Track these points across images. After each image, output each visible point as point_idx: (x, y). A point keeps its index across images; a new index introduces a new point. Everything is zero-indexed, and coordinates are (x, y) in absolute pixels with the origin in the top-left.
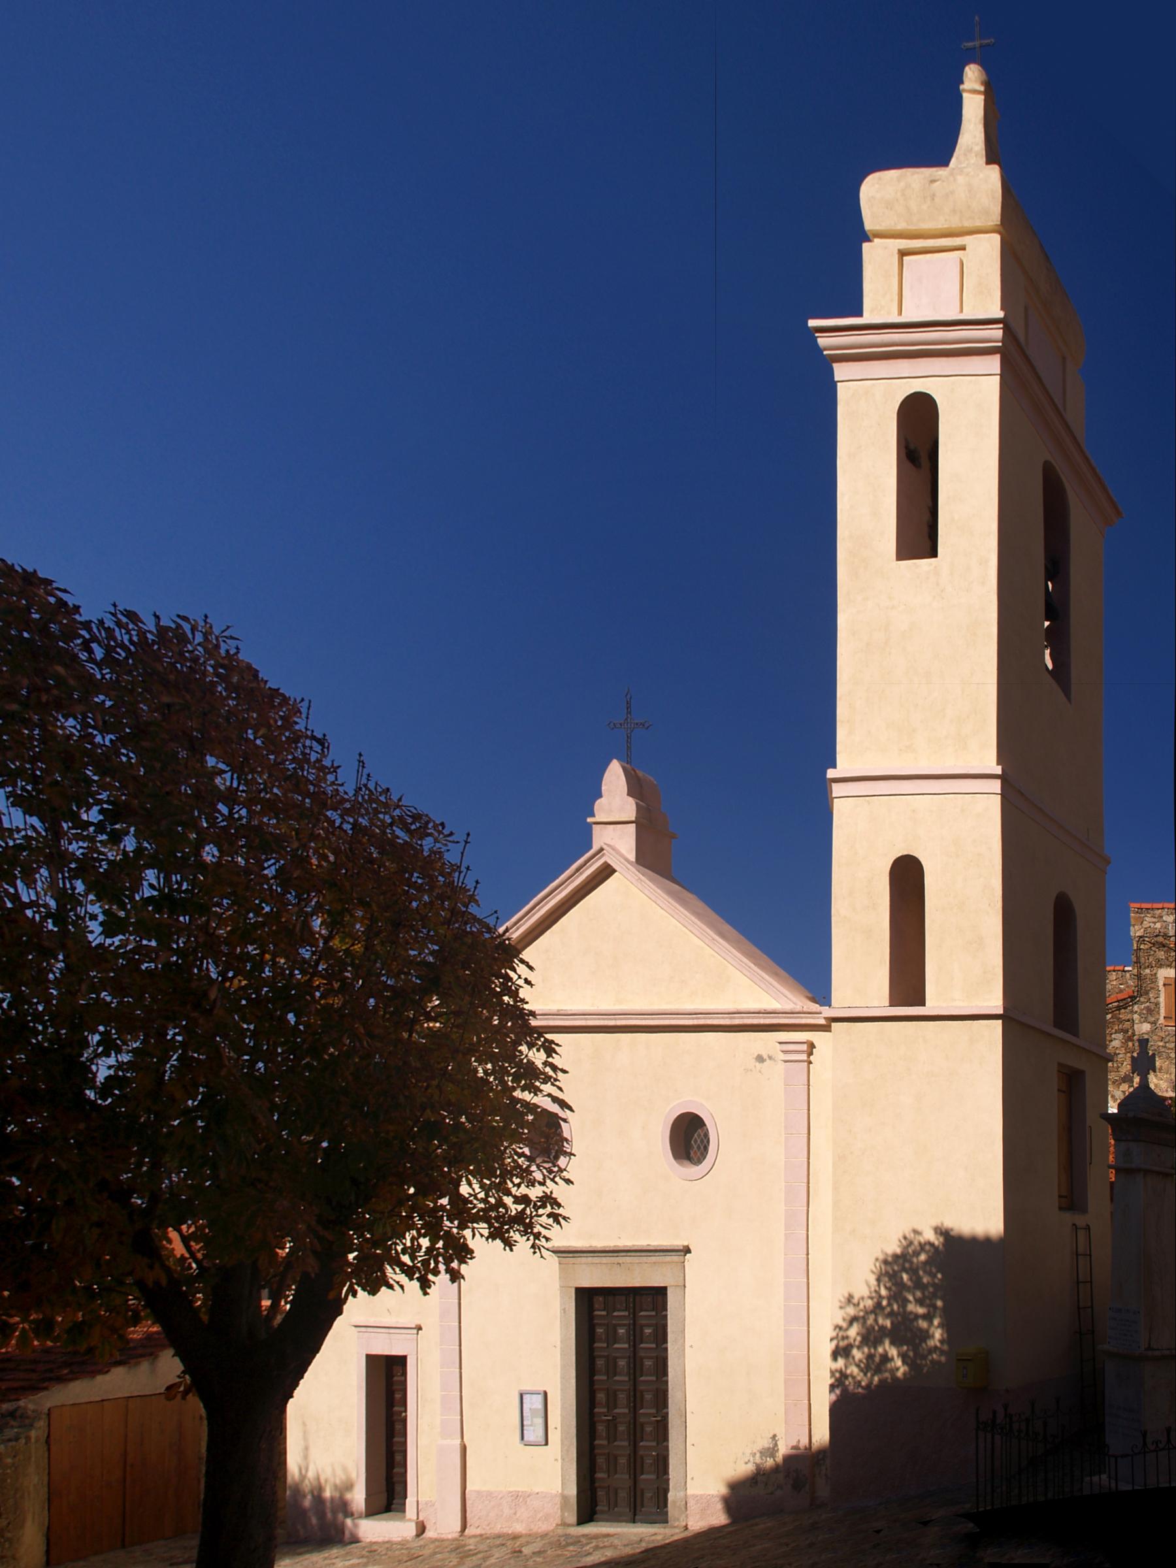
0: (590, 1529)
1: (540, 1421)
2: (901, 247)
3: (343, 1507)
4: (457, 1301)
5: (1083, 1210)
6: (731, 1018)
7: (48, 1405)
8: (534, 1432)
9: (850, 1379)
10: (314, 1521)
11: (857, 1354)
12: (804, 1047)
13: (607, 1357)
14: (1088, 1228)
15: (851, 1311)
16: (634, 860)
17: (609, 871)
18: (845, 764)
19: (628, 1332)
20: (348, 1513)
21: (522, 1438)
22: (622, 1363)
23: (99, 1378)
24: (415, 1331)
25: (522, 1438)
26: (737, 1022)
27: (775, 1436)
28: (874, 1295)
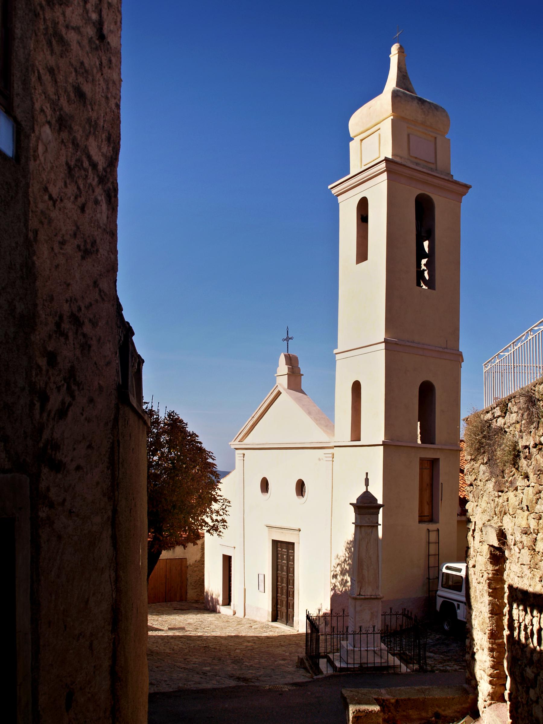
0: (275, 624)
3: (217, 602)
5: (437, 522)
8: (262, 588)
9: (337, 587)
10: (211, 604)
12: (331, 455)
13: (281, 565)
14: (438, 530)
15: (338, 561)
16: (287, 388)
18: (342, 345)
20: (219, 604)
22: (285, 568)
27: (321, 604)
28: (344, 555)
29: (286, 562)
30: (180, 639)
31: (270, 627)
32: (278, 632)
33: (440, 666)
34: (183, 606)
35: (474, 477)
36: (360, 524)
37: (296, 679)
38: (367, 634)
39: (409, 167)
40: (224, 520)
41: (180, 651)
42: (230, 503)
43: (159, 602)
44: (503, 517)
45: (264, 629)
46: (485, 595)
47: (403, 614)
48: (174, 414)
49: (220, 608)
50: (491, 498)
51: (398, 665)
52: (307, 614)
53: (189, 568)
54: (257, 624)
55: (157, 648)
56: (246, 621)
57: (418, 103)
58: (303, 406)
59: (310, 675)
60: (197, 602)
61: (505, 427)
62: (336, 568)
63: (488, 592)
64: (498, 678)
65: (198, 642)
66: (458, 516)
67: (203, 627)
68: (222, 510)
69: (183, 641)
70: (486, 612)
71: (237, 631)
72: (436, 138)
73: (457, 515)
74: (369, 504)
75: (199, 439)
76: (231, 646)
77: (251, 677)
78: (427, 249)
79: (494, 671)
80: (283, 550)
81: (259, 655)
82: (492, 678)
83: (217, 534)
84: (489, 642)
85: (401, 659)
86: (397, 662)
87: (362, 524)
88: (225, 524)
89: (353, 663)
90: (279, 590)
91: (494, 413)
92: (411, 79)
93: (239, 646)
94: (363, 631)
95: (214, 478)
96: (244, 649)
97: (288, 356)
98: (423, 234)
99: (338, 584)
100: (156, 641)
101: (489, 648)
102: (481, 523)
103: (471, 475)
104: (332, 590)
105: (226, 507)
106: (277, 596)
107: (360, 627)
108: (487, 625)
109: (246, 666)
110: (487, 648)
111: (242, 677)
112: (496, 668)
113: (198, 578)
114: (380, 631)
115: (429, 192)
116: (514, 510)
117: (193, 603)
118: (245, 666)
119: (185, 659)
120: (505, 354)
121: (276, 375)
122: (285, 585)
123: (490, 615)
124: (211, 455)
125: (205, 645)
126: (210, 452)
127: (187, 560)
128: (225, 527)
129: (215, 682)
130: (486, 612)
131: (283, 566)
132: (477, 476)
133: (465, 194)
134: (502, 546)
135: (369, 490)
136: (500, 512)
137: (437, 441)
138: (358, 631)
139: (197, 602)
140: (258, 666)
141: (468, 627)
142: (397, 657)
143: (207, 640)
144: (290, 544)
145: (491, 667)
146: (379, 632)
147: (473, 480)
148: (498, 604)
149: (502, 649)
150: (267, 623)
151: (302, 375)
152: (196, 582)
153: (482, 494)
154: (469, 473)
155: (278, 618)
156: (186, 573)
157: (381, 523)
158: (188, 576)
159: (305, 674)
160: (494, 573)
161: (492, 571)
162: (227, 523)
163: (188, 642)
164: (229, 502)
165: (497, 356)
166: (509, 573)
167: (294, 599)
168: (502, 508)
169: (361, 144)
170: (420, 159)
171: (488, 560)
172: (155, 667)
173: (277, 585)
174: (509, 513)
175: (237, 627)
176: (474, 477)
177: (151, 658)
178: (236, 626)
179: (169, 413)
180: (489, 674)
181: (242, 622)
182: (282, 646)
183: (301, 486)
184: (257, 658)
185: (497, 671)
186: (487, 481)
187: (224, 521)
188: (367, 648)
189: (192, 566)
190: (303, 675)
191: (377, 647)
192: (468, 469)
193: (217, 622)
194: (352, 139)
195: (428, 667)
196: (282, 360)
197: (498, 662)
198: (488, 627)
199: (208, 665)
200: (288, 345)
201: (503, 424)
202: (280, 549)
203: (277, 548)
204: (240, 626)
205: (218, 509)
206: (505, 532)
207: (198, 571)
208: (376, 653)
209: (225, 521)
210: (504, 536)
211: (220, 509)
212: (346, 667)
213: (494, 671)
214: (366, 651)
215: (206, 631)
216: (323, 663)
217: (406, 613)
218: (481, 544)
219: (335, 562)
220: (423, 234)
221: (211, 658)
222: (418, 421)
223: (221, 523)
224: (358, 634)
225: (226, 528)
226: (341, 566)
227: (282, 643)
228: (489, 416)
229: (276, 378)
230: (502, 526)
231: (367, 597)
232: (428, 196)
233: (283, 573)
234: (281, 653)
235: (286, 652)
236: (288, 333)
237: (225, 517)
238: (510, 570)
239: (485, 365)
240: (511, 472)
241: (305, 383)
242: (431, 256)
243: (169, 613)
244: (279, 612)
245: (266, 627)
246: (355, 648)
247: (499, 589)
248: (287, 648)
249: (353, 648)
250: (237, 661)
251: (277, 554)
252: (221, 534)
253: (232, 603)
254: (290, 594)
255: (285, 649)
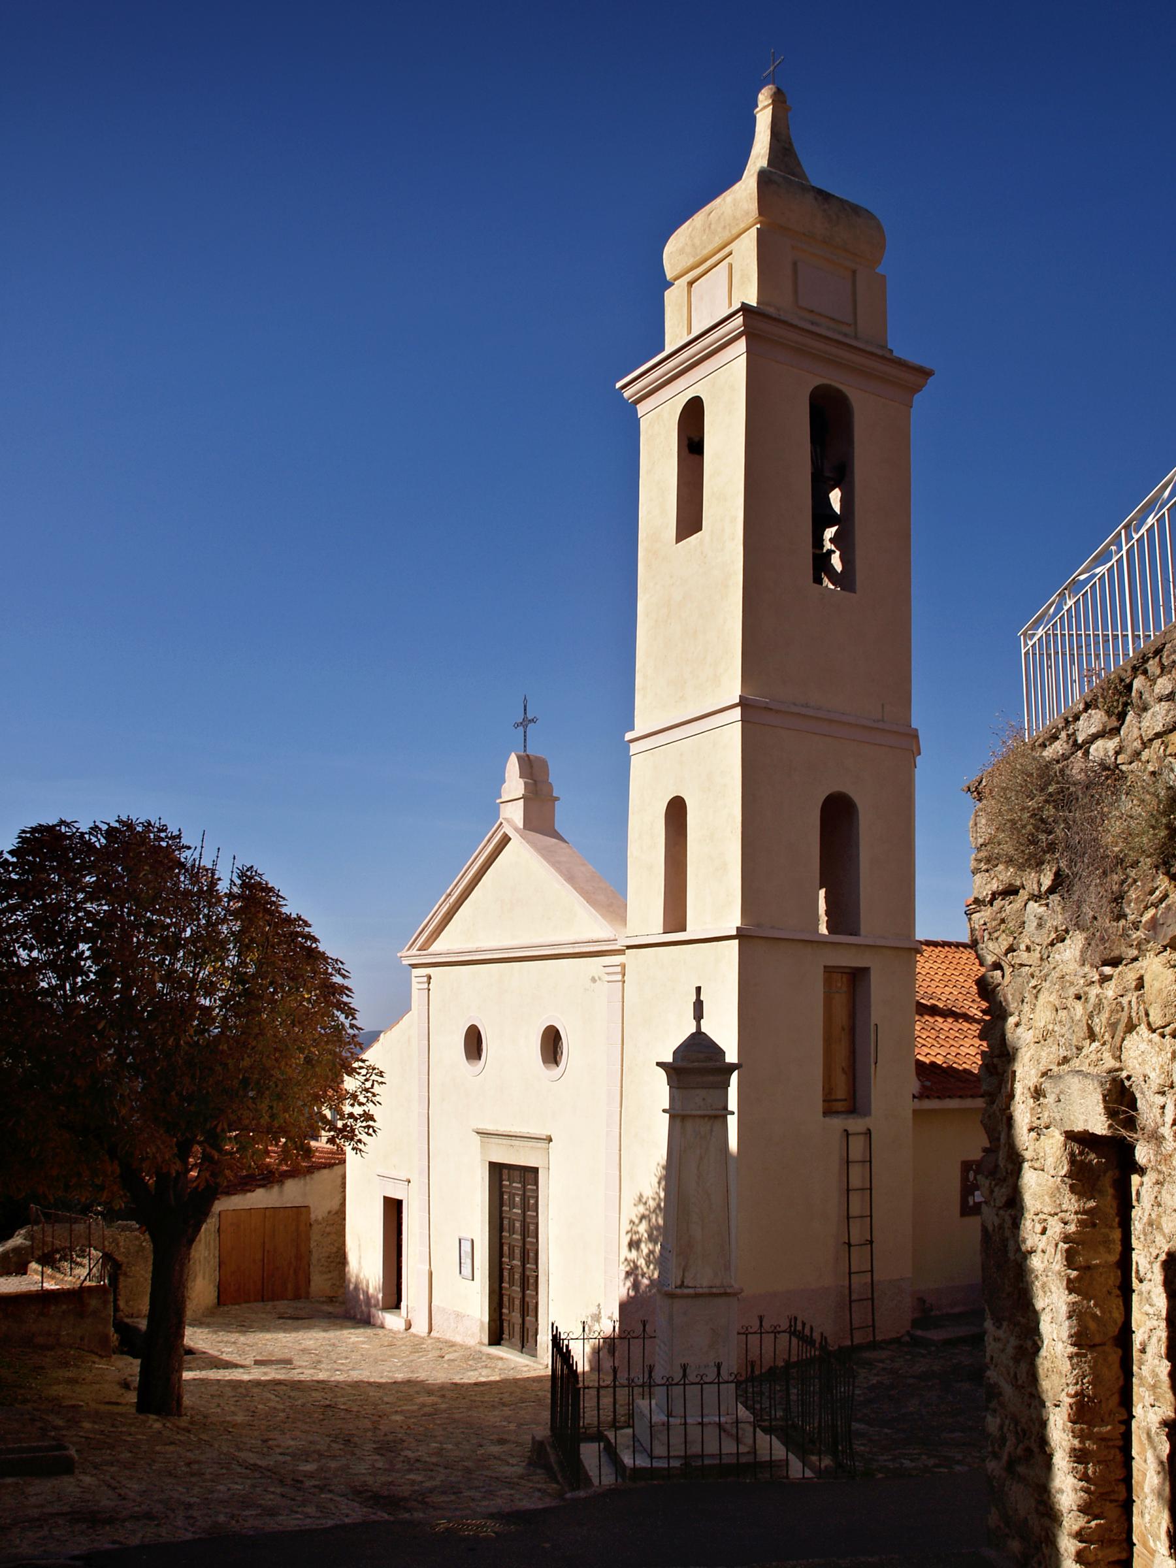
0: (495, 1351)
1: (469, 1261)
2: (689, 280)
4: (427, 1164)
6: (573, 947)
7: (219, 1209)
8: (467, 1270)
11: (645, 1248)
14: (868, 1133)
15: (641, 1209)
16: (522, 827)
17: (507, 839)
18: (643, 722)
19: (521, 1199)
21: (460, 1273)
22: (518, 1224)
23: (249, 1194)
24: (407, 1183)
25: (460, 1273)
26: (577, 950)
27: (599, 1305)
28: (656, 1196)
29: (520, 1211)
30: (276, 1388)
31: (484, 1358)
32: (500, 1369)
33: (886, 1458)
34: (301, 1309)
35: (1005, 943)
36: (680, 1112)
37: (520, 1499)
38: (702, 1384)
39: (792, 325)
40: (368, 1114)
41: (267, 1417)
42: (382, 1076)
43: (246, 1302)
44: (1123, 1040)
45: (470, 1363)
46: (1054, 1289)
47: (793, 1332)
48: (254, 873)
49: (384, 1318)
50: (1072, 991)
51: (780, 1461)
52: (555, 1333)
53: (315, 1228)
54: (455, 1351)
55: (219, 1410)
56: (432, 1344)
57: (816, 199)
58: (556, 865)
59: (559, 1487)
60: (332, 1301)
61: (1118, 762)
62: (638, 1226)
63: (1065, 1278)
64: (1102, 1542)
65: (314, 1394)
66: (915, 1100)
67: (334, 1357)
68: (364, 1092)
69: (281, 1392)
70: (1060, 1339)
71: (409, 1367)
72: (854, 272)
73: (911, 1096)
74: (705, 1064)
75: (313, 931)
76: (387, 1403)
77: (406, 1494)
78: (837, 507)
79: (1088, 1522)
80: (514, 1185)
81: (445, 1429)
82: (1084, 1545)
83: (351, 1146)
84: (1073, 1432)
85: (787, 1443)
86: (779, 1451)
87: (689, 1112)
88: (371, 1123)
89: (666, 1455)
90: (506, 1273)
91: (1074, 734)
92: (800, 157)
93: (406, 1405)
94: (692, 1377)
95: (342, 1017)
96: (413, 1412)
97: (526, 758)
98: (828, 474)
99: (642, 1262)
100: (219, 1393)
101: (1073, 1450)
102: (1033, 1072)
103: (997, 939)
104: (628, 1274)
105: (373, 1085)
106: (501, 1288)
107: (684, 1368)
108: (1064, 1381)
109: (407, 1460)
110: (1068, 1450)
111: (386, 1493)
112: (1097, 1511)
113: (335, 1250)
114: (733, 1376)
115: (841, 383)
116: (1166, 1010)
117: (323, 1302)
118: (403, 1462)
119: (265, 1441)
120: (1097, 570)
121: (498, 801)
122: (519, 1263)
123: (1074, 1350)
124: (340, 968)
125: (328, 1402)
126: (337, 960)
127: (309, 1211)
128: (371, 1131)
129: (311, 1510)
130: (1060, 1339)
131: (514, 1220)
132: (1015, 938)
133: (917, 389)
134: (1123, 1132)
135: (703, 1030)
136: (1113, 1026)
137: (864, 928)
138: (678, 1377)
139: (331, 1300)
140: (434, 1460)
141: (992, 1381)
142: (777, 1437)
143: (337, 1389)
144: (528, 1171)
145: (1079, 1511)
146: (731, 1379)
147: (1004, 951)
148: (1098, 1313)
149: (1113, 1452)
150: (478, 1348)
151: (557, 799)
152: (329, 1257)
153: (1034, 987)
154: (990, 933)
155: (504, 1336)
156: (309, 1239)
157: (736, 1111)
158: (313, 1244)
159: (544, 1486)
160: (1082, 1219)
161: (1076, 1213)
162: (375, 1121)
163: (291, 1394)
164: (381, 1074)
165: (1066, 592)
166: (1154, 1216)
167: (537, 1293)
168: (1118, 1011)
169: (689, 292)
170: (820, 315)
171: (1063, 1181)
172: (183, 1463)
173: (501, 1263)
174: (1149, 1024)
175: (411, 1358)
176: (1005, 943)
177: (182, 1438)
178: (408, 1356)
179: (242, 872)
180: (1074, 1532)
181: (423, 1346)
182: (504, 1404)
183: (554, 1041)
184: (438, 1439)
185: (1098, 1521)
186: (1052, 944)
187: (368, 1117)
188: (702, 1416)
189: (321, 1224)
190: (539, 1490)
191: (728, 1414)
192: (985, 924)
193: (366, 1346)
194: (670, 284)
195: (857, 1464)
196: (513, 766)
197: (1102, 1494)
198: (1068, 1385)
199: (316, 1456)
200: (525, 736)
201: (1111, 753)
202: (508, 1183)
203: (501, 1180)
204: (417, 1354)
205: (355, 1089)
206: (1131, 1086)
207: (335, 1233)
208: (725, 1431)
209: (371, 1118)
210: (1126, 1099)
211: (360, 1090)
212: (650, 1466)
213: (1088, 1522)
214: (700, 1427)
215: (338, 1368)
216: (589, 1453)
217: (799, 1328)
218: (1033, 1134)
219: (632, 1211)
220: (828, 474)
221: (329, 1436)
222: (821, 888)
223: (362, 1122)
224: (677, 1384)
225: (373, 1134)
226: (650, 1221)
227: (506, 1398)
228: (1058, 747)
229: (499, 807)
230: (1121, 1069)
231: (700, 1291)
232: (839, 391)
233: (514, 1236)
234: (498, 1424)
235: (510, 1422)
236: (525, 710)
237: (371, 1108)
238: (1159, 1205)
239: (1025, 634)
240: (1152, 893)
241: (562, 819)
242: (844, 521)
243: (265, 1328)
244: (505, 1324)
245: (476, 1356)
246: (670, 1419)
247: (1101, 1270)
248: (514, 1410)
249: (666, 1418)
250: (387, 1447)
251: (501, 1194)
252: (361, 1146)
253: (403, 1304)
254: (529, 1282)
255: (510, 1412)
